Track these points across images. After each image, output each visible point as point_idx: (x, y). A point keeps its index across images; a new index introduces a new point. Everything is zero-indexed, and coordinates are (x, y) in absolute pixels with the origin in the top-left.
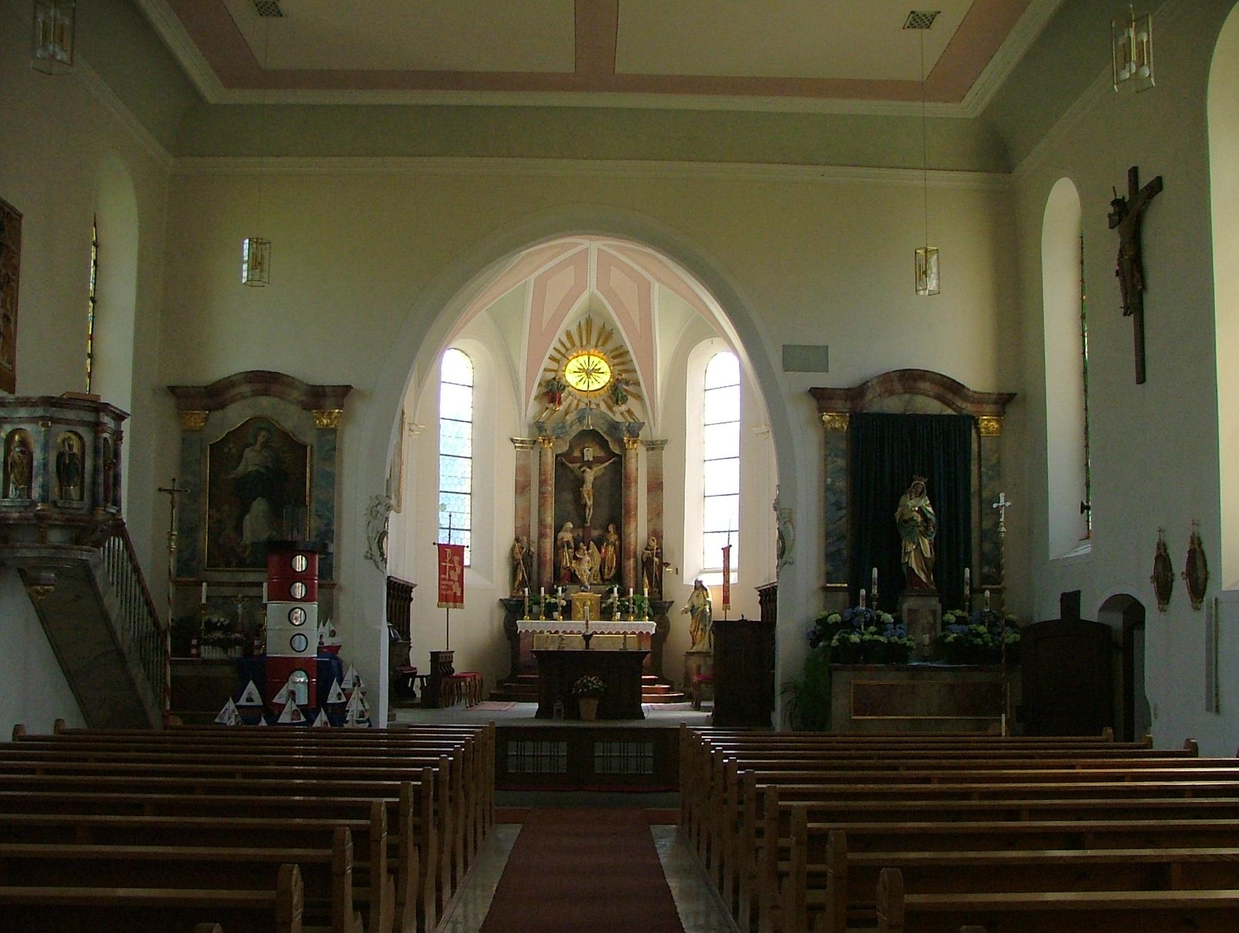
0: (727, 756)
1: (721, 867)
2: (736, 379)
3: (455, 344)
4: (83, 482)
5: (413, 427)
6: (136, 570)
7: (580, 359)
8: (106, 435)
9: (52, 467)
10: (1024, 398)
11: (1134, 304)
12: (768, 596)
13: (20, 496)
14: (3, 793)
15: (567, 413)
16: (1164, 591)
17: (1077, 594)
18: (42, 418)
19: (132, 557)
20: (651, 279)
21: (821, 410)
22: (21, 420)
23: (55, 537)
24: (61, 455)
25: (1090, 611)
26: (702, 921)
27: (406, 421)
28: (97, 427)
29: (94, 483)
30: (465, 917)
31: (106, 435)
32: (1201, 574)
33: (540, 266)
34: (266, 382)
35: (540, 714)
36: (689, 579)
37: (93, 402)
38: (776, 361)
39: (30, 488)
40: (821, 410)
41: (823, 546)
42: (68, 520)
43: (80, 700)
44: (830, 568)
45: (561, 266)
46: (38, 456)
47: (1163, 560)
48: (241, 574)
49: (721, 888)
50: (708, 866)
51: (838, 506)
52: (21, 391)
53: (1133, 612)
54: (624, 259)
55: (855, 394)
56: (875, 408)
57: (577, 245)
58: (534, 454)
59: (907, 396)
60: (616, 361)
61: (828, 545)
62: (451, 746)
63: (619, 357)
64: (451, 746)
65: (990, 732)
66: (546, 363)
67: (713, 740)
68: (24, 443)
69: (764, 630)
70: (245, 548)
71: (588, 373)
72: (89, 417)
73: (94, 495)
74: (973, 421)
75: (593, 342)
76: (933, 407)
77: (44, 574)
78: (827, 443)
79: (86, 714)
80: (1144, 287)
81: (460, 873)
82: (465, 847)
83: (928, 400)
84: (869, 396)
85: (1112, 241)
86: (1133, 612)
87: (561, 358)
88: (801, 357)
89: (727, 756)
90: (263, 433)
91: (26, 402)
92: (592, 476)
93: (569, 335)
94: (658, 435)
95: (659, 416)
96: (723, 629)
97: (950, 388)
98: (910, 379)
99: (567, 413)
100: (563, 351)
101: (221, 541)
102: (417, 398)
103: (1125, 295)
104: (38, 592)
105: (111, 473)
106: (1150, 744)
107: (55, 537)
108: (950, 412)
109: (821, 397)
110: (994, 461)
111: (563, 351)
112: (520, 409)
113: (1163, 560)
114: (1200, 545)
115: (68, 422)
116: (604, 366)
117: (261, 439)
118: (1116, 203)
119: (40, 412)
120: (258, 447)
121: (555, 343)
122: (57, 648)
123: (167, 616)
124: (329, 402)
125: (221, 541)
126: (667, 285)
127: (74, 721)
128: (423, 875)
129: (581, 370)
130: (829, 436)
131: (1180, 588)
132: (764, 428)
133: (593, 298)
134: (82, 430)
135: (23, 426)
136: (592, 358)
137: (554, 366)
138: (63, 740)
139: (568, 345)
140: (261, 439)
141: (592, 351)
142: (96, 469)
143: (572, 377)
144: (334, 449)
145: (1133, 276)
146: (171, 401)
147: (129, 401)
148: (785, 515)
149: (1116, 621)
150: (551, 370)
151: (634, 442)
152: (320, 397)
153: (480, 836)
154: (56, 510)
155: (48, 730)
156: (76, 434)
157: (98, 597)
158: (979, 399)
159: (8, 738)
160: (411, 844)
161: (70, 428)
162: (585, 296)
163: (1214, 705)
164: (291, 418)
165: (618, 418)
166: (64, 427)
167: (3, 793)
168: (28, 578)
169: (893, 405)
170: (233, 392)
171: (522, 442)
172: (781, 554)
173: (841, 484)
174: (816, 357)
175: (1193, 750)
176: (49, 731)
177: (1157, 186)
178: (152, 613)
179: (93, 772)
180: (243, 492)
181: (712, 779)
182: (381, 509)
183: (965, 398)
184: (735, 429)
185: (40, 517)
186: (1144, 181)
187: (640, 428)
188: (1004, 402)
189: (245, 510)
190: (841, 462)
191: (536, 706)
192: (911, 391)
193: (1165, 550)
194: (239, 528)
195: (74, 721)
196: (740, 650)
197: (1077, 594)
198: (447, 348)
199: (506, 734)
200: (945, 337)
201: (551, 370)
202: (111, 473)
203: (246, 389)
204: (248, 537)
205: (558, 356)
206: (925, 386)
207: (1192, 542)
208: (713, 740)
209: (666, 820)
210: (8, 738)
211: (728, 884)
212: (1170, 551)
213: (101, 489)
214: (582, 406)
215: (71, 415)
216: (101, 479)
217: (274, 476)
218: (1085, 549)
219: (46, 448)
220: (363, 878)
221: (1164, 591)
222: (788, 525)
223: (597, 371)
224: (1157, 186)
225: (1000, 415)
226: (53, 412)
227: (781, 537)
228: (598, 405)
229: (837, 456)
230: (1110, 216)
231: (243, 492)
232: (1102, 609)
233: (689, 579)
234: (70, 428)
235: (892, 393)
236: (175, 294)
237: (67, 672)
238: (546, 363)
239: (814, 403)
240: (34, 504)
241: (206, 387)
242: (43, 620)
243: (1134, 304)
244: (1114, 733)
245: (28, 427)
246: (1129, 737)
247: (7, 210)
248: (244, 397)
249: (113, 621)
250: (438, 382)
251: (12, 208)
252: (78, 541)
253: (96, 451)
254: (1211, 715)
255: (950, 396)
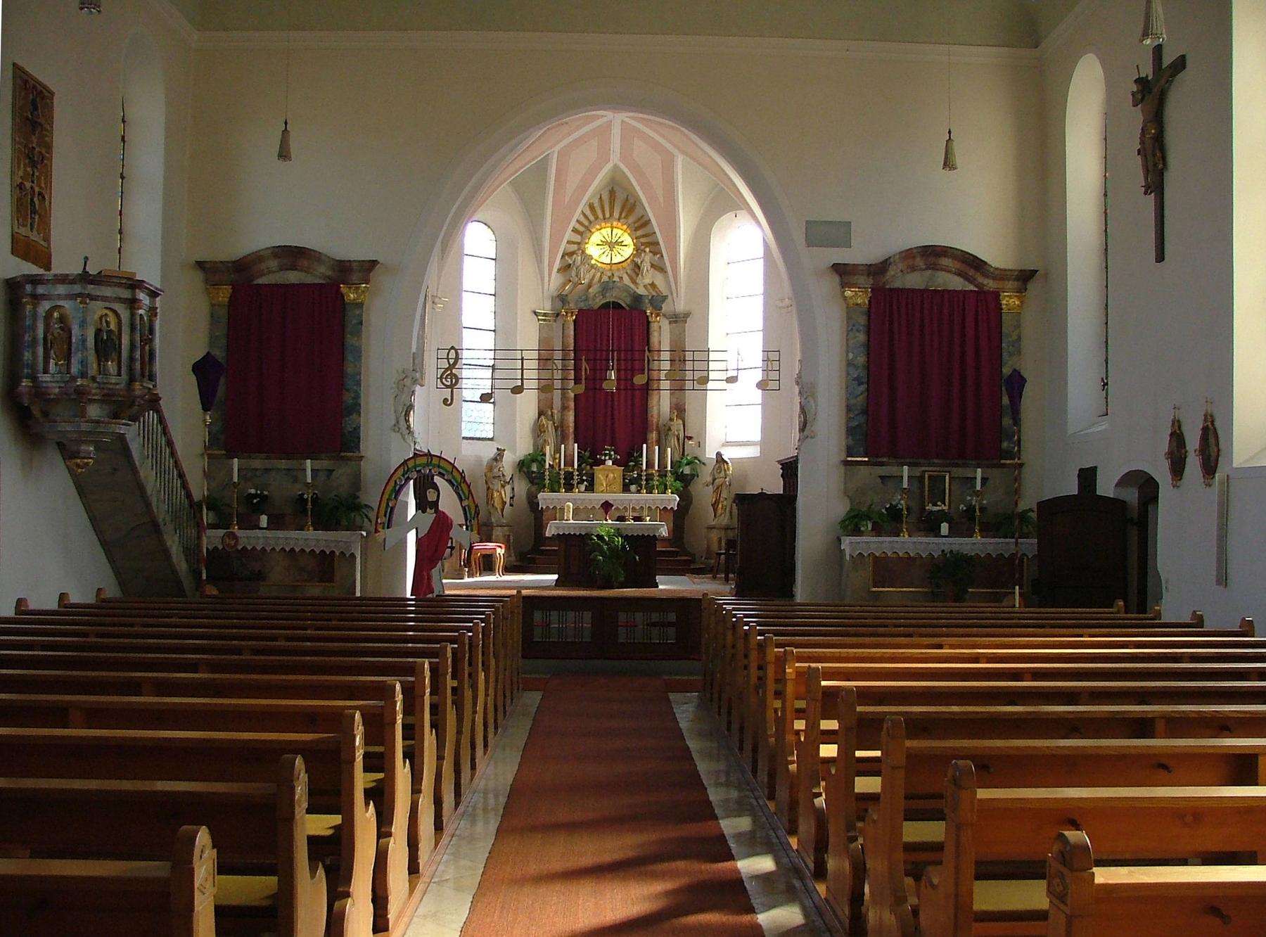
0: (747, 624)
1: (742, 729)
2: (760, 252)
3: (477, 216)
4: (120, 357)
5: (437, 300)
6: (170, 443)
7: (603, 231)
8: (141, 312)
9: (91, 342)
10: (1046, 274)
11: (1155, 184)
12: (789, 469)
13: (60, 372)
14: (4, 671)
15: (590, 286)
16: (1177, 468)
17: (1094, 469)
18: (80, 295)
19: (165, 432)
20: (675, 151)
21: (844, 285)
22: (59, 297)
23: (94, 411)
24: (98, 332)
25: (1106, 487)
26: (723, 779)
27: (429, 295)
28: (133, 303)
29: (131, 359)
30: (496, 775)
31: (141, 312)
32: (1213, 449)
33: (564, 138)
35: (558, 584)
36: (710, 454)
37: (128, 279)
38: (799, 236)
39: (69, 365)
40: (844, 285)
41: (844, 421)
42: (109, 395)
43: (117, 571)
44: (851, 442)
45: (582, 140)
46: (76, 331)
47: (1177, 437)
49: (741, 749)
50: (729, 729)
51: (858, 380)
52: (58, 267)
53: (1147, 486)
54: (645, 129)
55: (878, 269)
56: (897, 284)
57: (599, 117)
58: (557, 326)
59: (930, 272)
60: (639, 233)
61: (849, 420)
62: (482, 613)
63: (640, 227)
64: (482, 613)
65: (1004, 604)
66: (569, 235)
67: (734, 609)
68: (62, 319)
69: (787, 501)
71: (612, 245)
72: (126, 294)
73: (131, 369)
74: (996, 295)
75: (616, 215)
76: (956, 283)
77: (83, 447)
78: (849, 318)
79: (121, 583)
80: (1165, 164)
81: (491, 735)
82: (496, 710)
83: (951, 276)
84: (891, 272)
85: (1135, 118)
86: (1147, 486)
87: (584, 231)
88: (823, 233)
89: (747, 624)
91: (63, 279)
93: (592, 207)
94: (681, 307)
95: (682, 291)
96: (745, 501)
97: (972, 264)
98: (932, 255)
99: (590, 286)
100: (586, 223)
102: (440, 272)
103: (1147, 171)
104: (78, 466)
105: (147, 347)
106: (1158, 615)
107: (94, 411)
108: (972, 288)
109: (843, 271)
110: (1015, 337)
111: (586, 223)
112: (542, 280)
113: (1177, 437)
114: (1212, 422)
115: (105, 299)
116: (627, 239)
118: (1139, 81)
119: (77, 289)
121: (577, 215)
122: (93, 520)
123: (199, 489)
124: (355, 277)
126: (691, 157)
127: (112, 591)
128: (459, 732)
129: (604, 243)
130: (850, 309)
131: (1193, 464)
132: (787, 302)
133: (616, 166)
134: (117, 306)
135: (61, 303)
136: (615, 231)
137: (577, 238)
138: (102, 608)
139: (592, 218)
141: (615, 224)
142: (132, 346)
143: (594, 249)
144: (361, 323)
145: (1154, 155)
146: (199, 277)
147: (158, 273)
148: (807, 390)
149: (1131, 496)
150: (574, 243)
151: (658, 315)
153: (508, 701)
154: (95, 385)
155: (90, 599)
156: (115, 312)
157: (135, 471)
158: (1001, 275)
159: (9, 612)
160: (449, 701)
161: (107, 304)
162: (609, 166)
163: (1223, 579)
165: (641, 291)
166: (99, 303)
167: (4, 671)
168: (68, 452)
169: (914, 281)
170: (263, 266)
171: (545, 315)
172: (803, 427)
173: (861, 360)
174: (838, 233)
175: (1198, 621)
176: (53, 605)
177: (1180, 64)
178: (185, 485)
179: (137, 636)
181: (733, 647)
182: (408, 382)
183: (986, 275)
184: (759, 301)
185: (80, 392)
186: (1167, 60)
187: (663, 301)
188: (1025, 277)
190: (862, 337)
191: (556, 577)
192: (935, 267)
193: (1180, 427)
195: (112, 591)
196: (764, 521)
197: (1094, 469)
198: (470, 220)
199: (531, 603)
200: (971, 215)
201: (574, 243)
202: (147, 347)
203: (274, 264)
205: (581, 229)
206: (945, 262)
207: (1206, 420)
208: (734, 609)
209: (684, 688)
210: (9, 612)
211: (748, 746)
212: (1184, 428)
213: (138, 365)
214: (605, 278)
215: (108, 291)
216: (138, 355)
217: (295, 345)
218: (1103, 426)
219: (83, 324)
220: (411, 731)
221: (1177, 468)
222: (810, 399)
223: (620, 244)
224: (1180, 64)
225: (1021, 290)
226: (90, 289)
227: (803, 410)
228: (621, 278)
229: (858, 331)
230: (1133, 94)
232: (1118, 485)
233: (710, 454)
234: (107, 304)
235: (913, 269)
236: (204, 169)
237: (104, 543)
238: (569, 235)
239: (837, 279)
240: (74, 379)
241: (234, 262)
242: (81, 491)
243: (1155, 184)
244: (1126, 606)
245: (67, 304)
246: (1142, 608)
247: (39, 88)
249: (149, 493)
250: (461, 255)
251: (45, 87)
252: (116, 416)
253: (133, 328)
254: (1221, 588)
255: (971, 272)
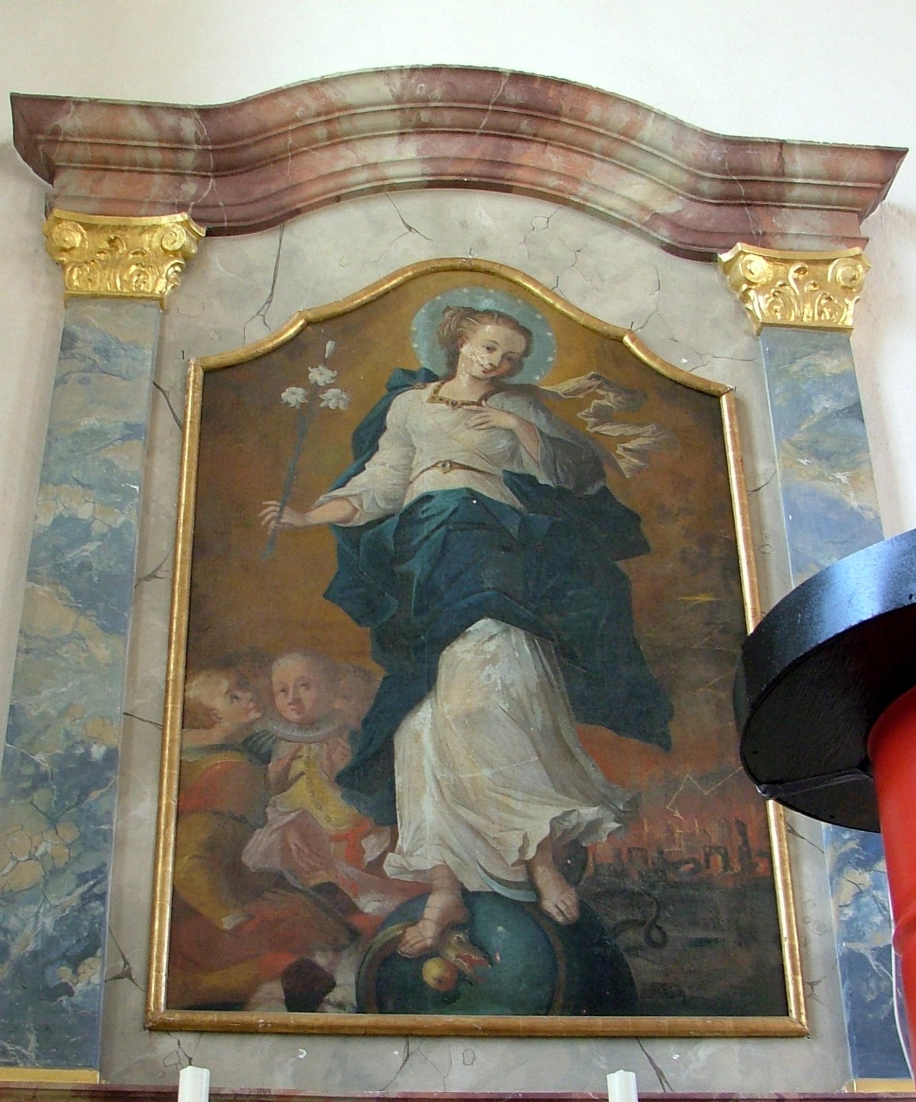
34: (501, 123)
48: (395, 1051)
70: (415, 894)
90: (489, 331)
92: (302, 1054)
101: (259, 851)
117: (476, 356)
120: (461, 386)
124: (795, 225)
125: (259, 851)
140: (476, 356)
144: (855, 411)
152: (744, 191)
164: (618, 280)
180: (401, 597)
189: (409, 682)
194: (370, 774)
203: (402, 156)
204: (428, 830)
231: (401, 597)
248: (384, 188)
